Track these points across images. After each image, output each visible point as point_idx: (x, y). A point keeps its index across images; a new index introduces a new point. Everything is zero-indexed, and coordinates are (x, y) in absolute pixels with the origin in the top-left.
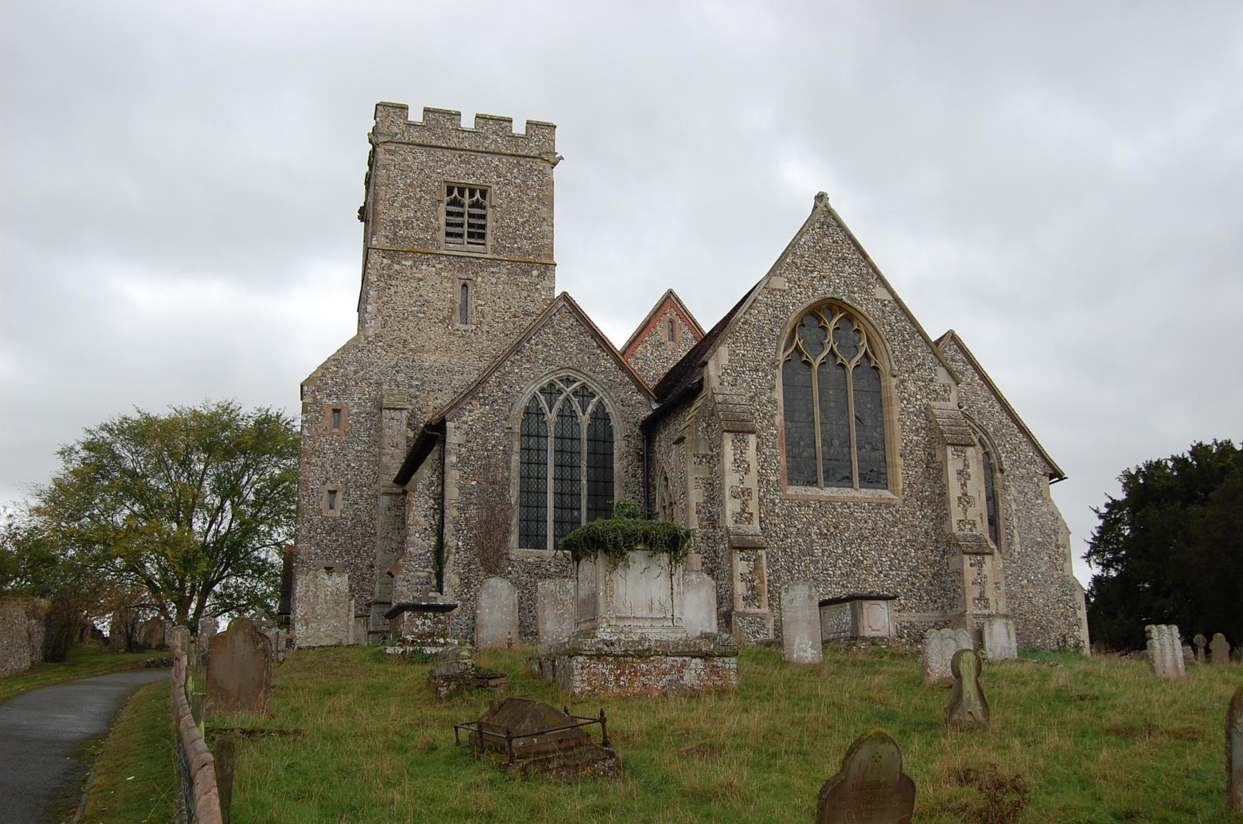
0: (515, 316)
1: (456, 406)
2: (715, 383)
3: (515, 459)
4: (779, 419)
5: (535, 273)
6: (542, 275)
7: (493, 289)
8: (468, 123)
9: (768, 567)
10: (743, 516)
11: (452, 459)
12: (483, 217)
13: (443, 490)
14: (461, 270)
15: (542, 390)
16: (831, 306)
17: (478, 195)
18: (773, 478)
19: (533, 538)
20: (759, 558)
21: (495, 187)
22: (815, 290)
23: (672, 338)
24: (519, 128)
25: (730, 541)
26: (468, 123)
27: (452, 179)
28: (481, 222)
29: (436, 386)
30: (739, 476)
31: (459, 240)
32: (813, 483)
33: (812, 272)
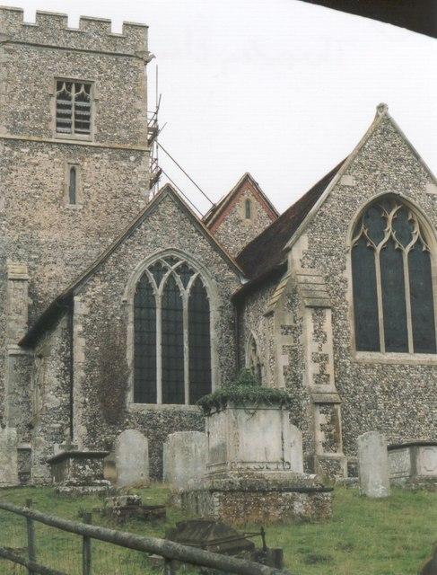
0: (116, 197)
1: (81, 283)
2: (297, 266)
3: (130, 328)
4: (349, 296)
5: (132, 158)
6: (138, 160)
7: (96, 171)
8: (73, 23)
9: (342, 419)
10: (321, 377)
11: (78, 328)
12: (88, 109)
13: (72, 354)
14: (70, 156)
15: (151, 268)
16: (388, 200)
17: (82, 90)
18: (344, 346)
19: (144, 394)
20: (335, 412)
21: (97, 82)
22: (377, 186)
23: (248, 216)
24: (117, 29)
25: (312, 398)
26: (73, 23)
27: (61, 75)
28: (86, 113)
29: (51, 260)
30: (304, 339)
31: (66, 129)
32: (377, 349)
33: (375, 171)
